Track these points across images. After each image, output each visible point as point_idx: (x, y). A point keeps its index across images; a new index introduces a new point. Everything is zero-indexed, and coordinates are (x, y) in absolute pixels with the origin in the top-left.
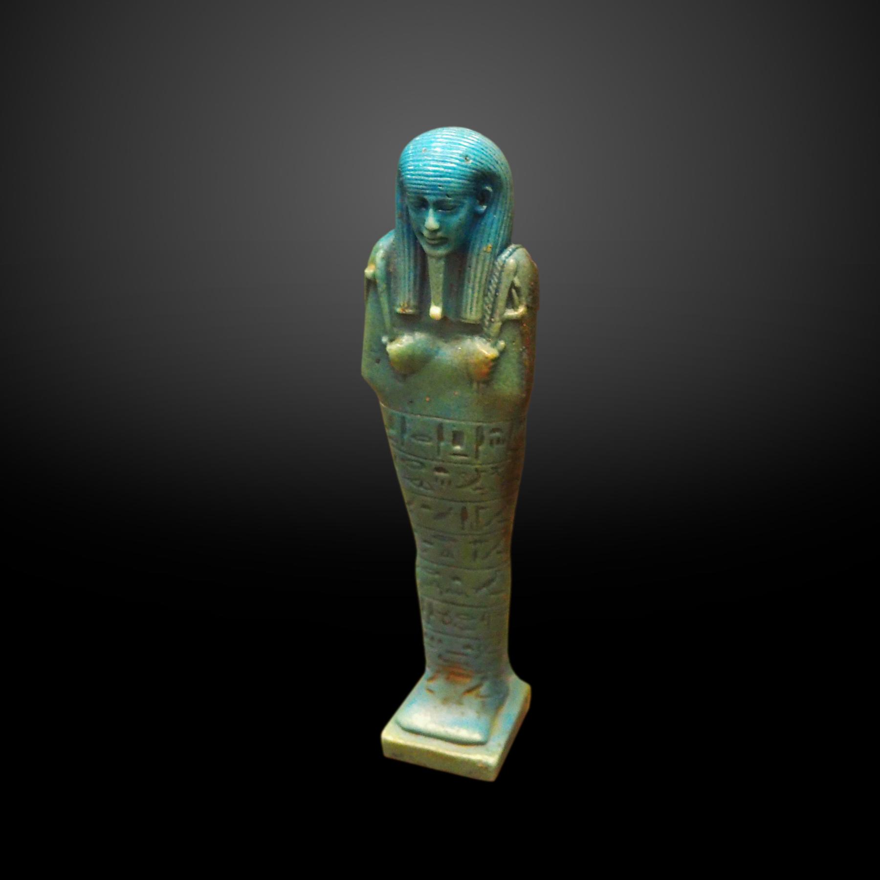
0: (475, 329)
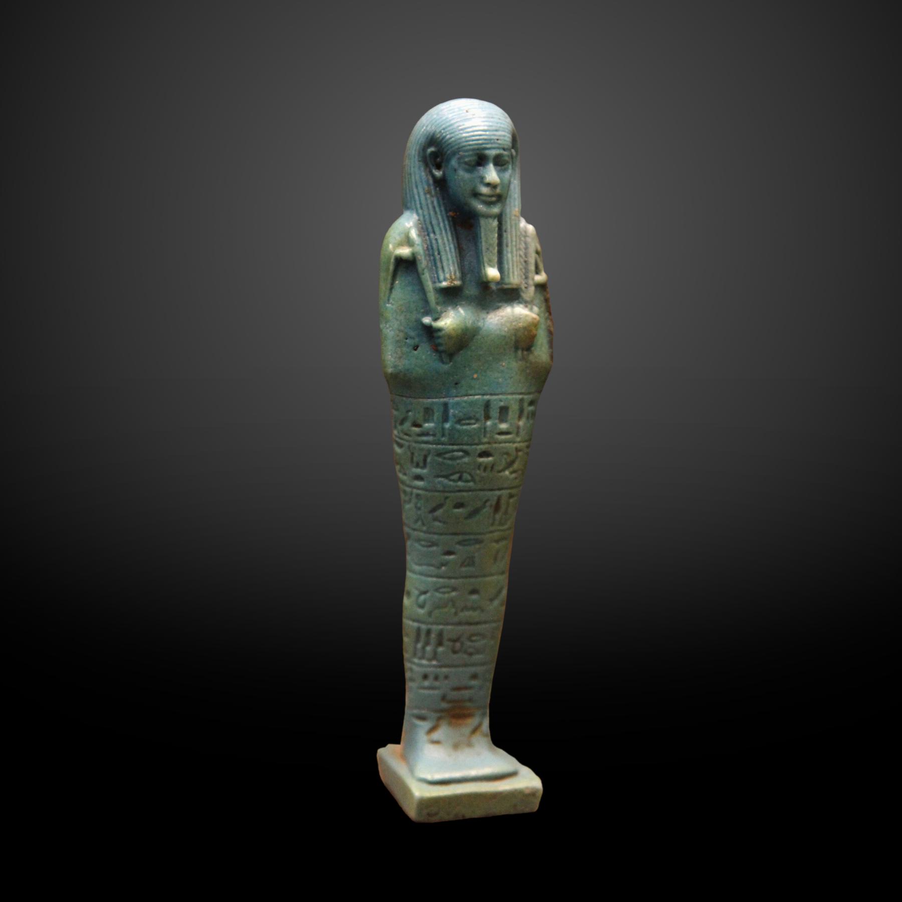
0: (511, 295)
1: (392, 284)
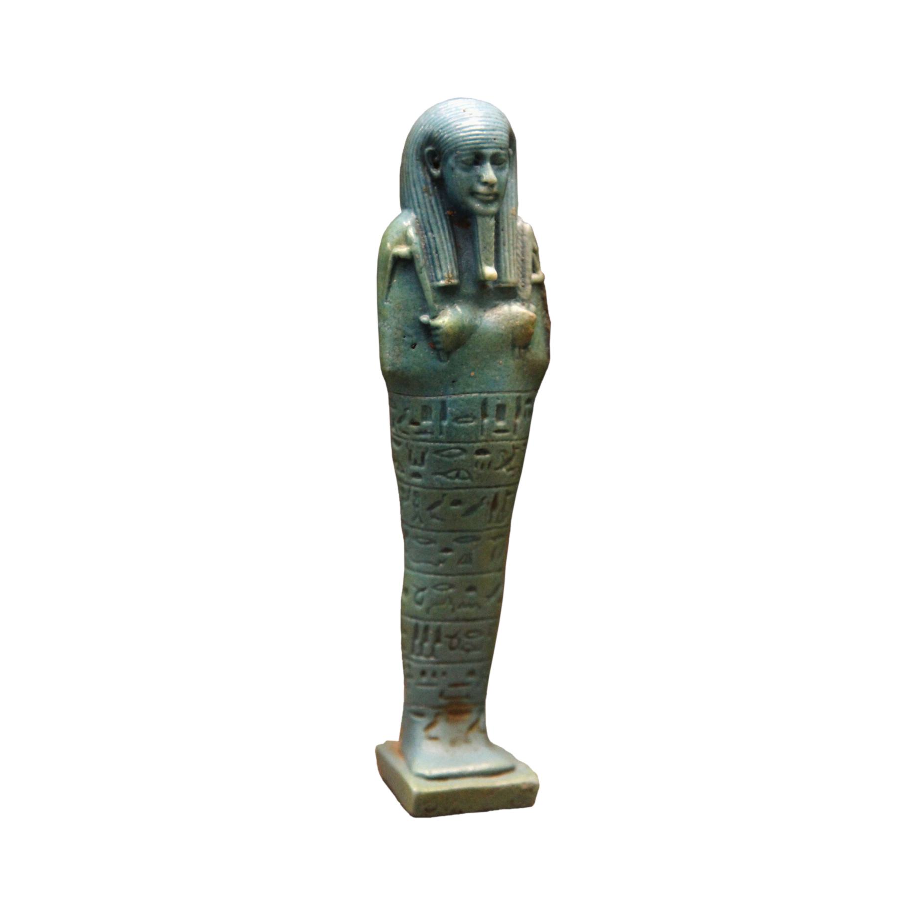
1: (390, 282)
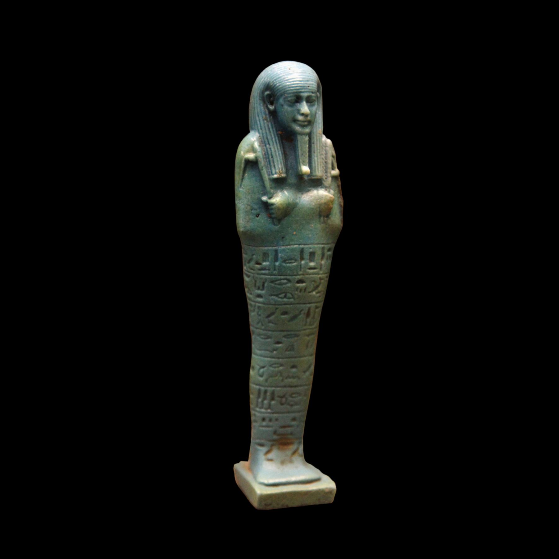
1: (243, 176)
